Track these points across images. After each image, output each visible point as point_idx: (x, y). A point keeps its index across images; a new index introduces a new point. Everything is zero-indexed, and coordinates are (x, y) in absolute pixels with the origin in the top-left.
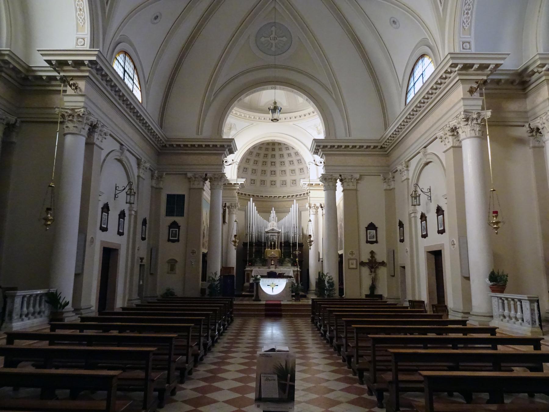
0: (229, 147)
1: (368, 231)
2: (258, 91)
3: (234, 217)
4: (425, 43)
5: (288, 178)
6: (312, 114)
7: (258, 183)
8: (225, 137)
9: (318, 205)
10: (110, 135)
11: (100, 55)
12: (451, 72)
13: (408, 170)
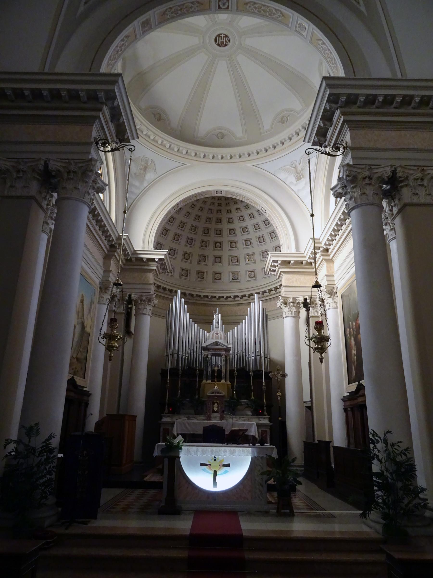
5: (243, 268)
7: (193, 275)
9: (301, 300)
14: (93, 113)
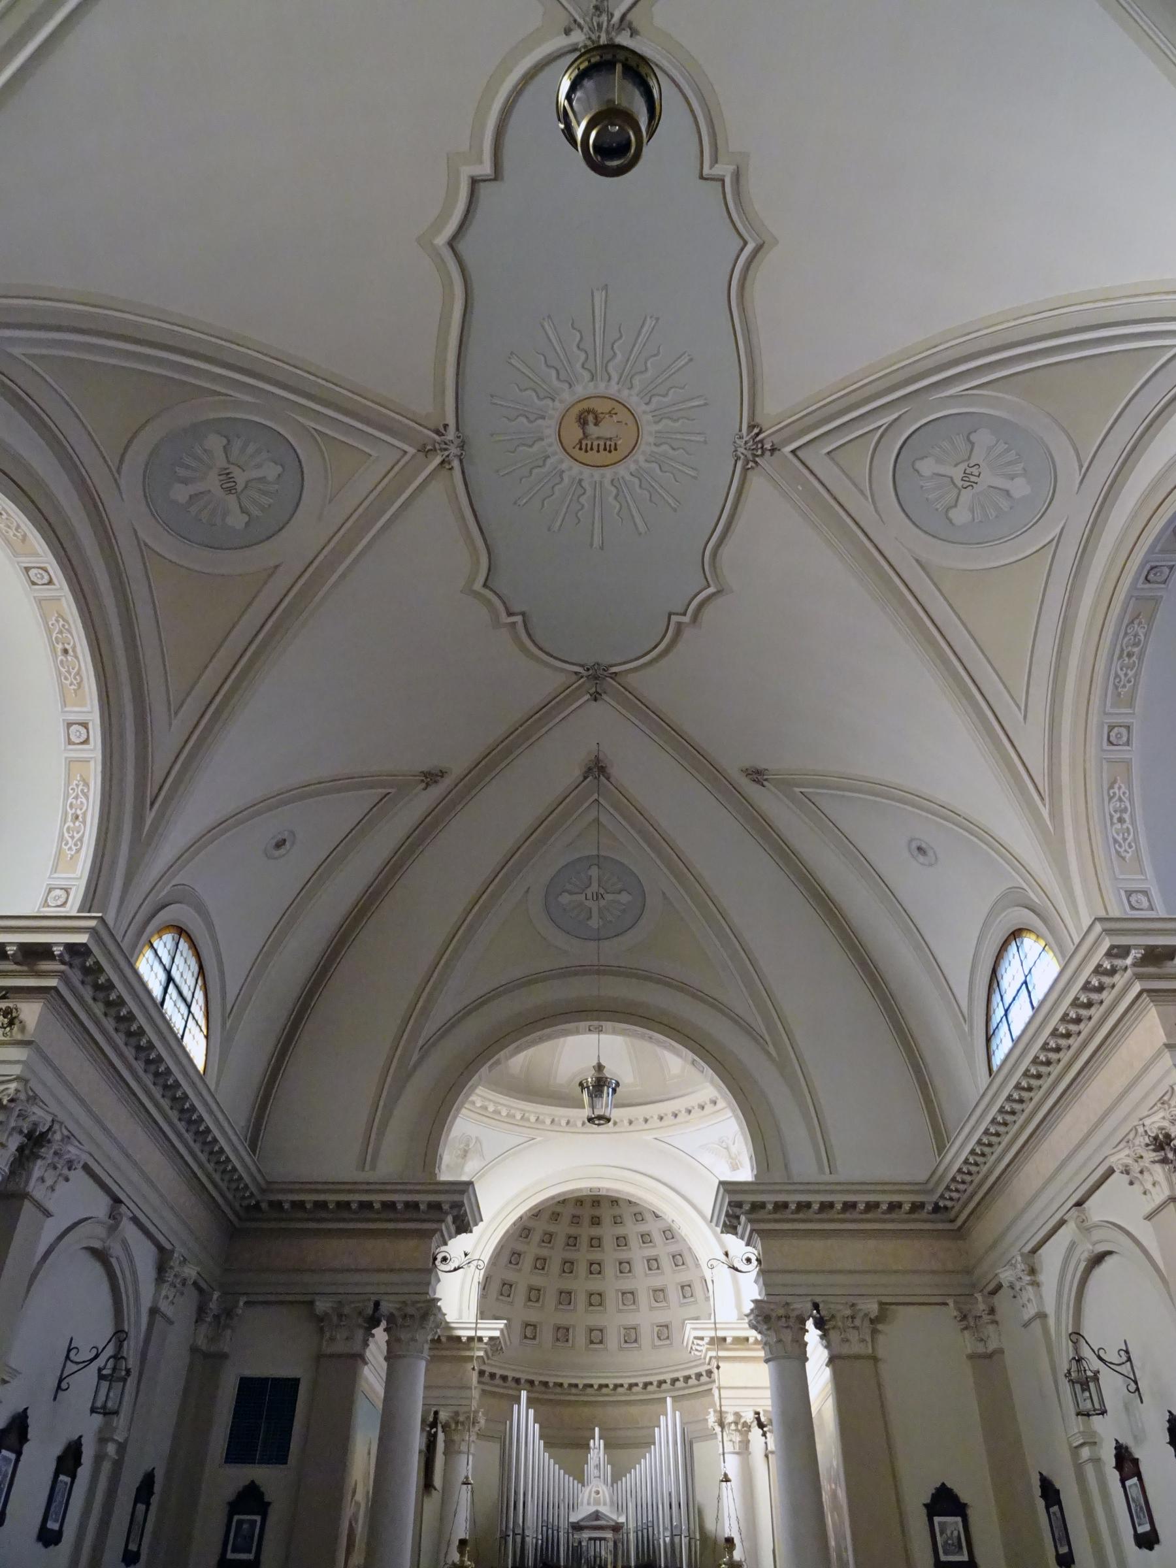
0: (454, 1210)
1: (937, 1520)
2: (549, 1037)
3: (465, 1466)
4: (1014, 898)
5: (645, 1317)
6: (709, 1108)
8: (445, 1176)
9: (749, 1417)
10: (86, 1168)
11: (103, 932)
12: (1112, 972)
13: (1036, 1284)
14: (434, 1226)
